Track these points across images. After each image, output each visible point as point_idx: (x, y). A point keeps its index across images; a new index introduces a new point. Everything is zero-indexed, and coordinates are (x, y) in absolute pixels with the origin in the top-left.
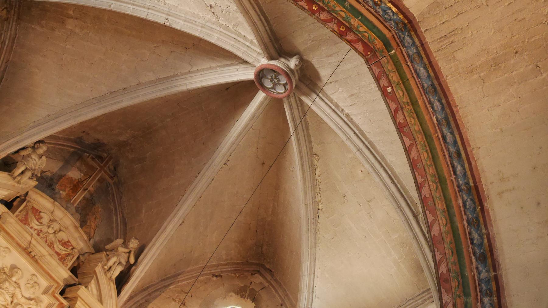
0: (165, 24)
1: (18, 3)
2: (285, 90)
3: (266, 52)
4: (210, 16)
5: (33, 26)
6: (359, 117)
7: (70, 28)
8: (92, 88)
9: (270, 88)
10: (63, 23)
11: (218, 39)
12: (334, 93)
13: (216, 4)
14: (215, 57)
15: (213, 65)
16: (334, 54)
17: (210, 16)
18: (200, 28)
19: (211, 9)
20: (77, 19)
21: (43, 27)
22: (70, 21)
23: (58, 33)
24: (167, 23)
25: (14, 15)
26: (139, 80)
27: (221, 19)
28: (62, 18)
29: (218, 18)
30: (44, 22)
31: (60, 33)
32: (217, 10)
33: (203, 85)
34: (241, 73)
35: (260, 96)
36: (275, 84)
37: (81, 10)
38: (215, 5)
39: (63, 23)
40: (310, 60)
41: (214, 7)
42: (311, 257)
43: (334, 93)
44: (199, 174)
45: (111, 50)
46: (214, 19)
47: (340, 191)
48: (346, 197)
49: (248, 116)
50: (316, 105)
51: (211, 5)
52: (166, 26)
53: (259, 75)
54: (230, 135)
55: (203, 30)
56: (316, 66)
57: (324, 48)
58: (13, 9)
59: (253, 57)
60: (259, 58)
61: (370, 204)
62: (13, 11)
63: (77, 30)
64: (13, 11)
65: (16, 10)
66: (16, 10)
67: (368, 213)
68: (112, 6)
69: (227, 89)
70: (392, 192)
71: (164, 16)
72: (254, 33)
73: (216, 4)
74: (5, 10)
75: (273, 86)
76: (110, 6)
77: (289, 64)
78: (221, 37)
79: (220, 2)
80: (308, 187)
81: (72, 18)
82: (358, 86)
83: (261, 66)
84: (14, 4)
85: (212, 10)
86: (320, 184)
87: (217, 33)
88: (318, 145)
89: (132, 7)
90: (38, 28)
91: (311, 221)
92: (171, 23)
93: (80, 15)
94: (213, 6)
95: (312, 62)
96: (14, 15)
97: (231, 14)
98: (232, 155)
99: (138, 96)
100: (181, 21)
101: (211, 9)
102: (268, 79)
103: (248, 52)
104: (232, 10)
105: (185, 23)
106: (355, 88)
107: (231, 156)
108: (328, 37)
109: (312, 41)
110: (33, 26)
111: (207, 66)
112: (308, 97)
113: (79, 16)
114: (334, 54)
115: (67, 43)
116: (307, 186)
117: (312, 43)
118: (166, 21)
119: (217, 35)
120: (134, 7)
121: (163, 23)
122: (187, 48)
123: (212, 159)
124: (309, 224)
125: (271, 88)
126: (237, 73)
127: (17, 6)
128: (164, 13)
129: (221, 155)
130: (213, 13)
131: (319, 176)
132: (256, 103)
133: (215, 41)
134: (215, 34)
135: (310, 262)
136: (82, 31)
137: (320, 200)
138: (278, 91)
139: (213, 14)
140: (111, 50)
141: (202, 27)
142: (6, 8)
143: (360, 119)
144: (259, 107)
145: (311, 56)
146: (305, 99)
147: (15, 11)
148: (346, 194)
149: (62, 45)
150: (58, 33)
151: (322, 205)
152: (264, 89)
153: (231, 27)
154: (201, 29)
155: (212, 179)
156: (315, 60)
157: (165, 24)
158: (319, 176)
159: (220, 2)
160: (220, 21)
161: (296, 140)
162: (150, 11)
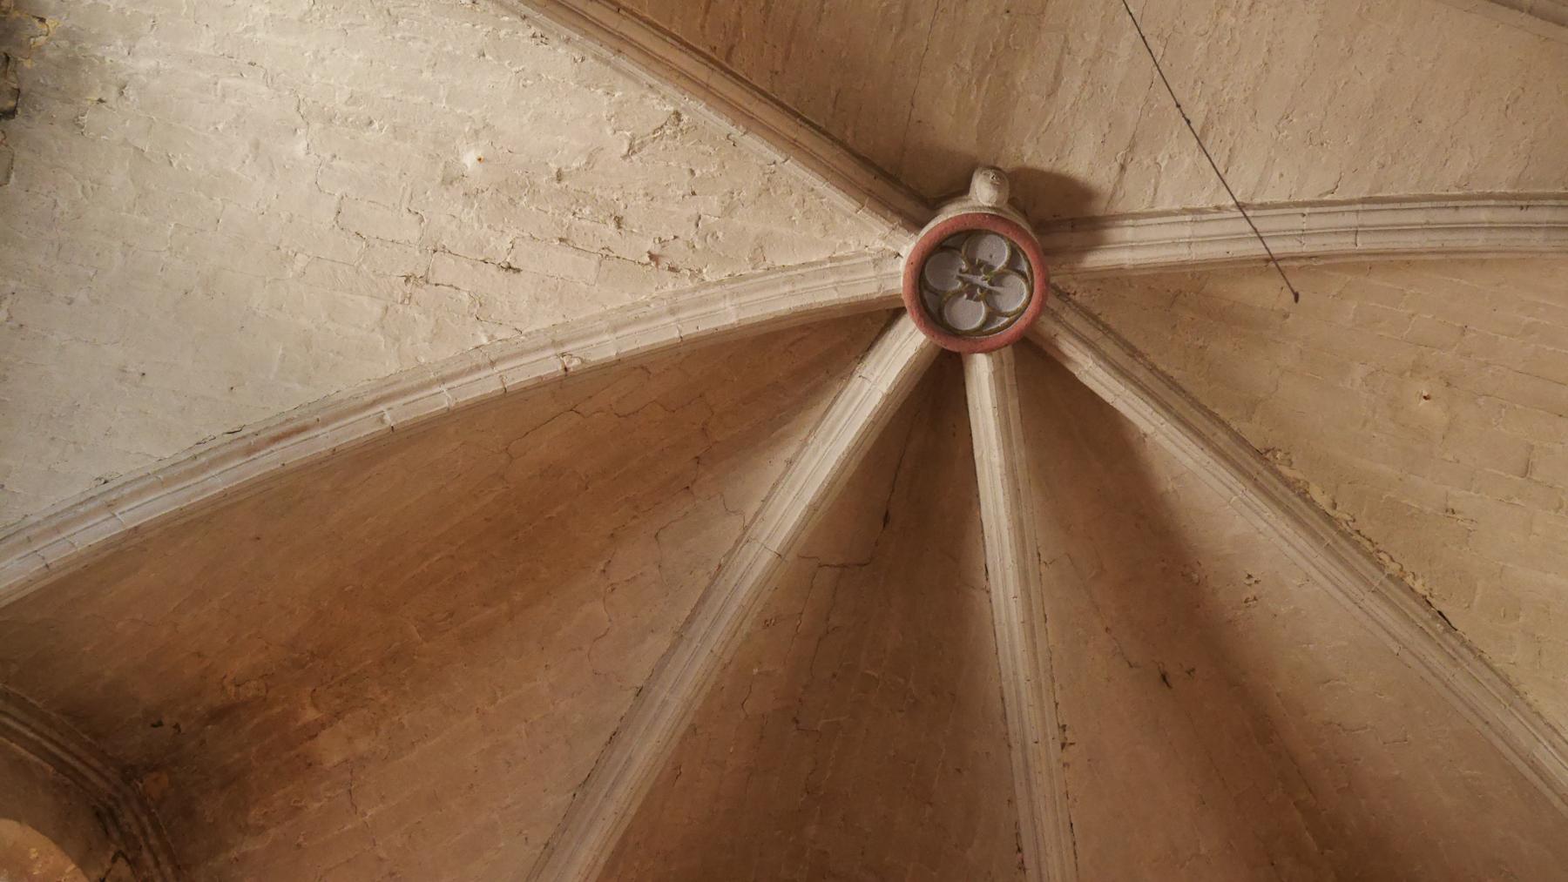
0: (566, 369)
1: (145, 819)
2: (1027, 281)
3: (889, 212)
4: (670, 285)
5: (234, 854)
6: (1276, 174)
7: (336, 759)
8: (521, 833)
9: (986, 323)
10: (310, 765)
11: (740, 307)
12: (1156, 190)
13: (660, 239)
14: (780, 431)
15: (790, 451)
16: (1059, 63)
17: (670, 285)
18: (669, 320)
19: (657, 264)
20: (338, 715)
21: (262, 829)
22: (324, 738)
23: (317, 805)
24: (570, 362)
25: (157, 864)
26: (631, 688)
27: (705, 271)
28: (298, 756)
29: (695, 274)
30: (254, 815)
31: (320, 801)
32: (675, 253)
33: (807, 503)
34: (877, 374)
35: (982, 374)
36: (988, 297)
37: (332, 678)
38: (659, 246)
39: (310, 765)
40: (1018, 163)
41: (664, 253)
42: (1536, 728)
43: (1156, 190)
44: (1019, 850)
45: (493, 703)
46: (690, 284)
47: (1428, 509)
48: (1459, 512)
49: (1001, 499)
50: (1139, 246)
51: (652, 257)
52: (574, 375)
53: (927, 310)
54: (1000, 615)
55: (681, 316)
56: (1046, 166)
57: (1023, 78)
58: (143, 844)
59: (870, 278)
60: (889, 270)
61: (1535, 478)
62: (146, 855)
63: (362, 745)
64: (146, 855)
65: (152, 841)
66: (152, 841)
67: (1557, 511)
68: (387, 417)
69: (886, 519)
70: (1547, 223)
71: (550, 352)
72: (813, 169)
73: (660, 239)
74: (121, 860)
75: (987, 304)
76: (382, 421)
77: (976, 204)
78: (744, 299)
79: (664, 226)
80: (1336, 542)
81: (323, 726)
82: (1195, 82)
83: (910, 263)
84: (136, 831)
85: (664, 263)
86: (1355, 526)
87: (725, 297)
88: (1250, 419)
89: (444, 388)
90: (252, 845)
91: (1434, 630)
92: (581, 355)
93: (339, 696)
94: (656, 251)
95: (1030, 164)
96: (157, 864)
97: (720, 234)
98: (1058, 700)
99: (665, 703)
100: (606, 337)
101: (657, 264)
102: (959, 294)
103: (846, 278)
104: (713, 219)
105: (619, 334)
106: (1191, 99)
107: (1057, 704)
108: (1006, 17)
109: (979, 83)
110: (234, 854)
111: (780, 466)
112: (1101, 249)
113: (338, 701)
114: (1059, 63)
115: (360, 809)
116: (1329, 541)
117: (985, 87)
118: (565, 359)
119: (728, 304)
120: (449, 385)
121: (560, 368)
122: (688, 488)
123: (1013, 745)
124: (1438, 640)
125: (990, 318)
126: (867, 385)
127: (149, 830)
128: (544, 348)
129: (1027, 694)
130: (672, 269)
131: (1334, 506)
132: (987, 434)
133: (738, 316)
134: (721, 305)
135: (1550, 742)
136: (377, 734)
137: (1401, 570)
138: (1013, 309)
139: (674, 274)
140: (493, 703)
141: (672, 312)
142: (118, 854)
143: (1282, 175)
144: (1007, 445)
145: (1013, 149)
146: (1098, 260)
147: (150, 848)
148: (1451, 504)
149: (349, 826)
150: (317, 805)
151: (1420, 581)
152: (978, 339)
153: (746, 270)
154: (673, 319)
155: (1068, 825)
156: (1033, 154)
157: (566, 369)
158: (1334, 506)
159: (664, 226)
160: (707, 279)
161: (1178, 426)
162: (500, 367)
